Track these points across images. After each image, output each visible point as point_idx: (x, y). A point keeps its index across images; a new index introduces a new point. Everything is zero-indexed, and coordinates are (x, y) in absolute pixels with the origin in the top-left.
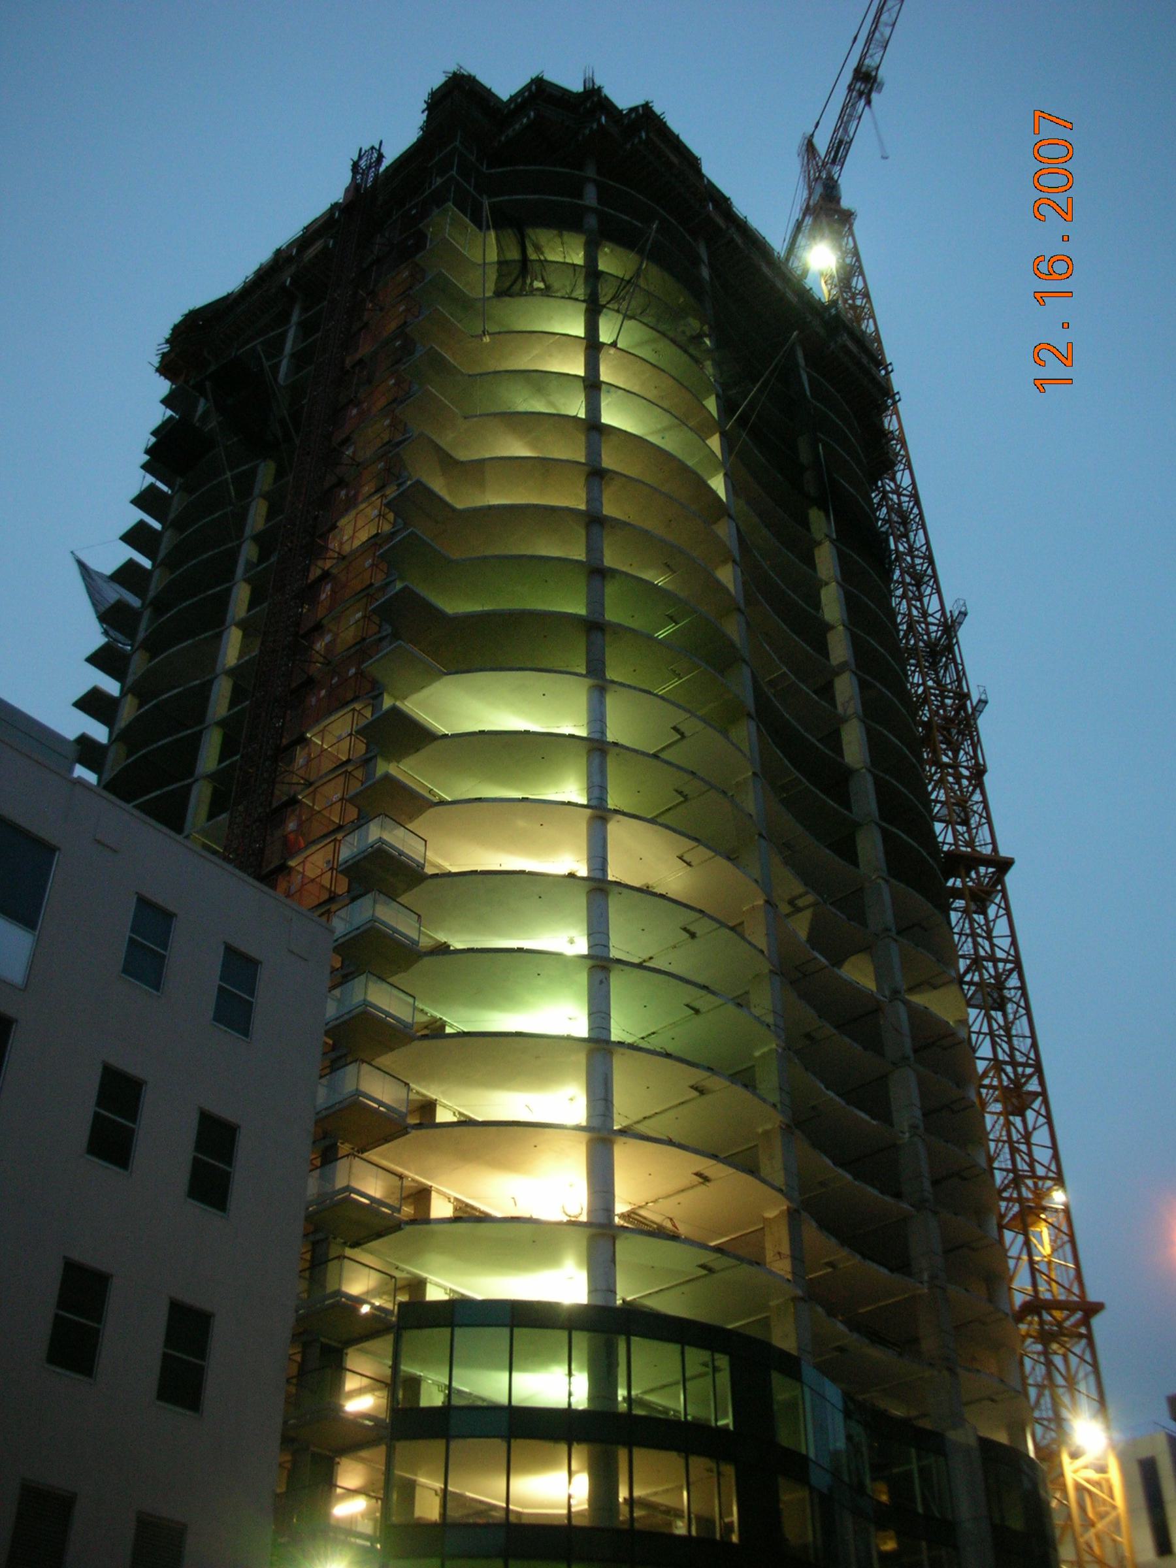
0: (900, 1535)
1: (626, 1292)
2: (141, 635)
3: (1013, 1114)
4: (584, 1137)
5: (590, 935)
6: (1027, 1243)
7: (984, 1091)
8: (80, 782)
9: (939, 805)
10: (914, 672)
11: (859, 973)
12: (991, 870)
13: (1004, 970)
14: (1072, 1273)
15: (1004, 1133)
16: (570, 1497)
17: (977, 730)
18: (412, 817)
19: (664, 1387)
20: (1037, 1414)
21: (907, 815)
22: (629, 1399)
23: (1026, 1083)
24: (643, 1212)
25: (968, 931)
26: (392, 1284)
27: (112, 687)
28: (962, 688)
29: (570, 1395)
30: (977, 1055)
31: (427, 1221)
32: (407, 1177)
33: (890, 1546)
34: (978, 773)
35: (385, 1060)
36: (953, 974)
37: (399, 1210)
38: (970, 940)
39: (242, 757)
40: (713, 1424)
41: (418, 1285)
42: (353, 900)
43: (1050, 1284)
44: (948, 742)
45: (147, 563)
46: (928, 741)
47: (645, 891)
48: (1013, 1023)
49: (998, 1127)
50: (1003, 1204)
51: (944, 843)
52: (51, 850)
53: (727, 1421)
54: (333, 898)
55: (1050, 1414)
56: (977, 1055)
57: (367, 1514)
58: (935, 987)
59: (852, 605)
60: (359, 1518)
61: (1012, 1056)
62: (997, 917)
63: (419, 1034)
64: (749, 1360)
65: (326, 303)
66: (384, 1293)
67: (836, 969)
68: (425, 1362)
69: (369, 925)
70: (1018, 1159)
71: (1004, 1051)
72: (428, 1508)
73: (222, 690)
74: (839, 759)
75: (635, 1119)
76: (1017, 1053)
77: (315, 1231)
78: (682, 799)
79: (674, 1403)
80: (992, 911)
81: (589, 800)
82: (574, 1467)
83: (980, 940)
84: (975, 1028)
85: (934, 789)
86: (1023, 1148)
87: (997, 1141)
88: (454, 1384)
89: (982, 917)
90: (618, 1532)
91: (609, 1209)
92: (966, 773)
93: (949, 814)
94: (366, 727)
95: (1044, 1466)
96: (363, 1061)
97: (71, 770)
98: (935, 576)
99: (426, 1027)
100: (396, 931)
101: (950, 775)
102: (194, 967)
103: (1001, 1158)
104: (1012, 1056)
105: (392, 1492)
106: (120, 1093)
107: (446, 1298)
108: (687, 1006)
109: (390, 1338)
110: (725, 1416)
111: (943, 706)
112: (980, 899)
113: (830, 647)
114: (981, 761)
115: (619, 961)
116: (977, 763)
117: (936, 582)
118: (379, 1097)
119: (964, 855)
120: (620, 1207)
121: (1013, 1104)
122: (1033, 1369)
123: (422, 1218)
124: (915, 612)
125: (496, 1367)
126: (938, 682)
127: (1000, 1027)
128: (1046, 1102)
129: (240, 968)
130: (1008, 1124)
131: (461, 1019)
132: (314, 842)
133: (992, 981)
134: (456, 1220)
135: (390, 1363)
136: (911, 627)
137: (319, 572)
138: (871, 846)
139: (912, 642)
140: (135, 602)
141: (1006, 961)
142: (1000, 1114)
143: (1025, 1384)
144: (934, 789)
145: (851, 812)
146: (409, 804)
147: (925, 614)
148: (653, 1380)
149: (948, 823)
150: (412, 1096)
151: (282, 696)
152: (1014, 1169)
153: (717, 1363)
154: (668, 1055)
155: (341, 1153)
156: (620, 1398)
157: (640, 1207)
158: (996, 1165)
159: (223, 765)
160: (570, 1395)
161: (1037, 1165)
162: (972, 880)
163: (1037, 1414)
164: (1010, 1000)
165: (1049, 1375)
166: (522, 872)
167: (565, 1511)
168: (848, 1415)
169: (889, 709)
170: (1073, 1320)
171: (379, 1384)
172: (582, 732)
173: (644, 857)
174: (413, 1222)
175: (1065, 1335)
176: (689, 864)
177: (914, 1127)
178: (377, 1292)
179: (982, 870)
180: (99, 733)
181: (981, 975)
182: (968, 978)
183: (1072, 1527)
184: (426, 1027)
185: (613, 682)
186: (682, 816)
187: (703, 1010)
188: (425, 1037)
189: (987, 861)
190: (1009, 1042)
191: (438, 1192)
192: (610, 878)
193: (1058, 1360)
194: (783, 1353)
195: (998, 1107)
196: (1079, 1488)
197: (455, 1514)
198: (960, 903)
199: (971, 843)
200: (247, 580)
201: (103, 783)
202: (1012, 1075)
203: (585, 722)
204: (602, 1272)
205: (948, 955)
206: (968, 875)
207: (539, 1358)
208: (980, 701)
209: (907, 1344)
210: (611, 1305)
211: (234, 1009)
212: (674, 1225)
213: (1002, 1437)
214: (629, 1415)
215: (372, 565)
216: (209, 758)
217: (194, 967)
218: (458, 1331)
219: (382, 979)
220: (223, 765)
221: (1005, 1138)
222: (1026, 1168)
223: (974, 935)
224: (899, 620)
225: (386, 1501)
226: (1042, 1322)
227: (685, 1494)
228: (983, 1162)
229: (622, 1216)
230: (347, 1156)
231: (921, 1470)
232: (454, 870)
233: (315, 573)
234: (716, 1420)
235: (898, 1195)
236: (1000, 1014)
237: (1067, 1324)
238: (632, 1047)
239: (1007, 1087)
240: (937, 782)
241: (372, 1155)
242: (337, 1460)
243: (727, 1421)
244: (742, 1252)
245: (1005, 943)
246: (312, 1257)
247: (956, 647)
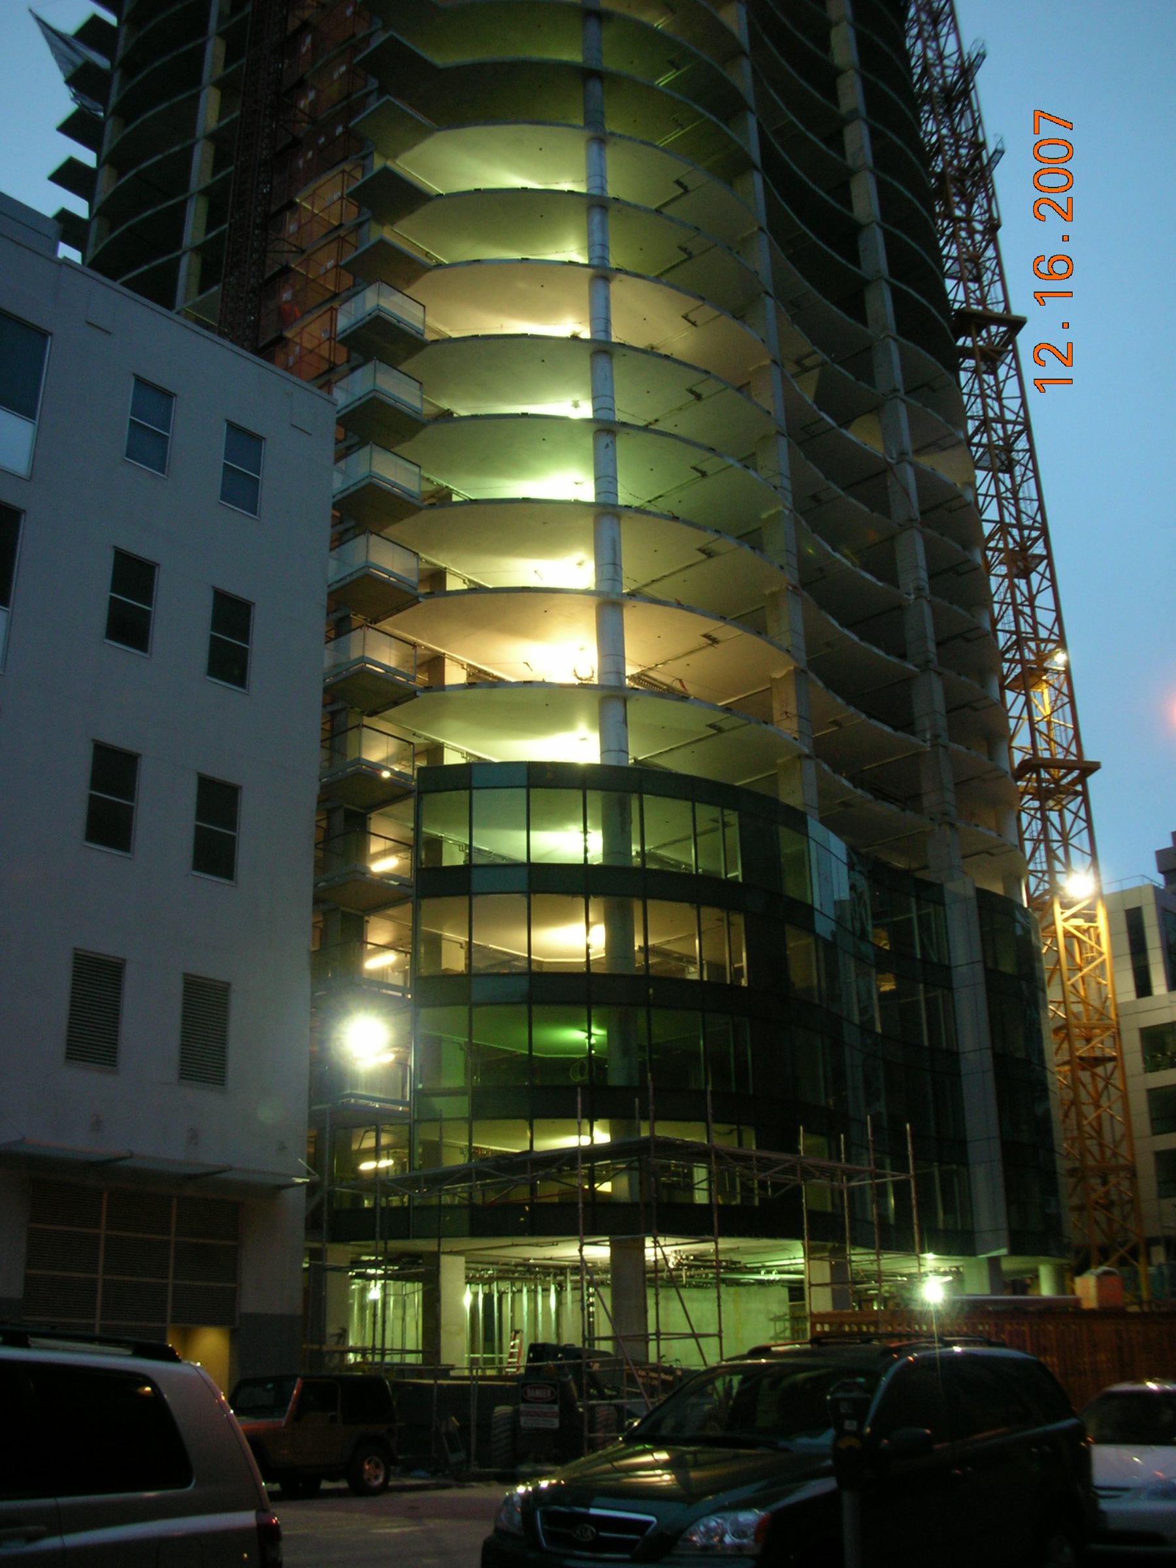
0: (898, 978)
1: (638, 751)
2: (113, 100)
3: (1019, 577)
4: (593, 601)
5: (594, 399)
6: (1028, 703)
7: (989, 554)
8: (67, 262)
9: (950, 262)
10: (928, 119)
11: (864, 436)
12: (1002, 329)
13: (1013, 432)
14: (1071, 733)
15: (1008, 595)
16: (588, 947)
17: (991, 181)
18: (409, 282)
19: (675, 842)
20: (1031, 867)
21: (918, 271)
22: (642, 854)
23: (1031, 546)
24: (652, 674)
25: (977, 392)
26: (408, 749)
27: (88, 158)
28: (977, 138)
29: (586, 851)
30: (984, 517)
31: (442, 687)
32: (420, 645)
33: (888, 987)
34: (993, 226)
35: (393, 531)
36: (962, 436)
37: (414, 679)
38: (979, 400)
39: (230, 225)
40: (723, 877)
41: (436, 750)
42: (353, 370)
43: (1049, 744)
44: (962, 194)
45: (112, 19)
46: (941, 193)
47: (650, 352)
48: (1020, 485)
49: (1002, 589)
50: (1006, 665)
51: (955, 301)
52: (44, 334)
53: (737, 873)
54: (332, 368)
55: (1045, 867)
56: (984, 517)
57: (396, 967)
58: (943, 449)
59: (865, 48)
60: (390, 971)
61: (1018, 519)
62: (1007, 378)
63: (426, 503)
64: (759, 816)
65: (226, 226)
66: (403, 759)
67: (844, 431)
68: (446, 824)
69: (371, 395)
70: (1022, 620)
71: (1010, 514)
72: (454, 960)
73: (202, 157)
74: (849, 214)
75: (643, 583)
76: (1024, 516)
77: (327, 800)
78: (686, 256)
79: (686, 857)
80: (1002, 371)
81: (590, 259)
82: (591, 920)
83: (989, 401)
84: (982, 490)
85: (945, 245)
86: (1027, 610)
87: (1002, 603)
88: (475, 844)
89: (992, 377)
90: (632, 978)
91: (620, 673)
92: (979, 227)
93: (961, 271)
94: (358, 189)
95: (1037, 915)
96: (372, 533)
97: (55, 250)
98: (952, 12)
99: (432, 496)
100: (394, 485)
101: (963, 229)
102: (198, 444)
103: (1005, 620)
104: (1018, 519)
105: (420, 946)
106: (133, 576)
107: (463, 761)
108: (694, 468)
109: (411, 803)
110: (736, 869)
111: (957, 155)
112: (990, 359)
113: (839, 93)
114: (995, 215)
115: (624, 424)
116: (991, 216)
117: (954, 20)
118: (389, 567)
119: (975, 314)
120: (630, 670)
121: (1018, 567)
122: (1030, 824)
123: (437, 684)
124: (930, 54)
125: (517, 827)
126: (953, 131)
127: (1007, 490)
128: (1050, 565)
129: (244, 443)
130: (1012, 587)
131: (467, 488)
132: (309, 312)
133: (1001, 443)
134: (470, 685)
135: (412, 825)
136: (926, 70)
137: (297, 23)
138: (881, 304)
139: (926, 87)
140: (103, 63)
141: (1015, 423)
142: (1004, 577)
143: (1022, 840)
144: (945, 245)
145: (859, 268)
146: (402, 269)
147: (941, 56)
148: (666, 836)
149: (959, 279)
150: (423, 566)
151: (271, 153)
152: (1017, 631)
153: (726, 819)
154: (675, 518)
155: (355, 624)
156: (634, 853)
157: (650, 669)
158: (999, 627)
159: (218, 177)
160: (586, 851)
161: (1040, 628)
162: (982, 339)
163: (1031, 867)
164: (1018, 462)
165: (1044, 830)
166: (525, 336)
167: (584, 960)
168: (851, 867)
169: (902, 157)
170: (1070, 778)
171: (403, 846)
172: (580, 188)
173: (649, 318)
174: (428, 689)
175: (1061, 793)
176: (694, 324)
177: (919, 589)
178: (398, 759)
179: (993, 329)
180: (80, 207)
181: (989, 437)
182: (976, 440)
183: (1060, 970)
184: (432, 496)
185: (612, 134)
186: (688, 270)
187: (709, 473)
188: (432, 505)
189: (998, 320)
190: (1016, 505)
191: (452, 659)
192: (614, 340)
193: (1054, 816)
194: (791, 810)
195: (1003, 570)
196: (1068, 935)
197: (480, 965)
198: (970, 363)
199: (982, 301)
200: (221, 35)
201: (88, 261)
202: (1018, 538)
203: (584, 177)
204: (613, 739)
205: (959, 415)
206: (979, 334)
207: (555, 818)
208: (996, 151)
209: (911, 799)
210: (623, 764)
211: (241, 488)
212: (683, 686)
213: (998, 889)
214: (642, 871)
215: (354, 13)
216: (194, 230)
217: (198, 444)
218: (475, 792)
219: (387, 449)
220: (218, 177)
221: (1009, 601)
222: (1029, 630)
223: (983, 396)
224: (913, 63)
225: (414, 955)
226: (1039, 780)
227: (697, 942)
228: (987, 625)
229: (632, 678)
230: (361, 627)
231: (920, 918)
232: (455, 335)
233: (293, 24)
234: (726, 874)
235: (903, 656)
236: (1007, 476)
237: (1064, 782)
238: (639, 510)
239: (1012, 550)
240: (949, 237)
241: (385, 625)
242: (366, 918)
243: (737, 873)
244: (753, 708)
245: (1015, 405)
246: (332, 726)
247: (973, 93)
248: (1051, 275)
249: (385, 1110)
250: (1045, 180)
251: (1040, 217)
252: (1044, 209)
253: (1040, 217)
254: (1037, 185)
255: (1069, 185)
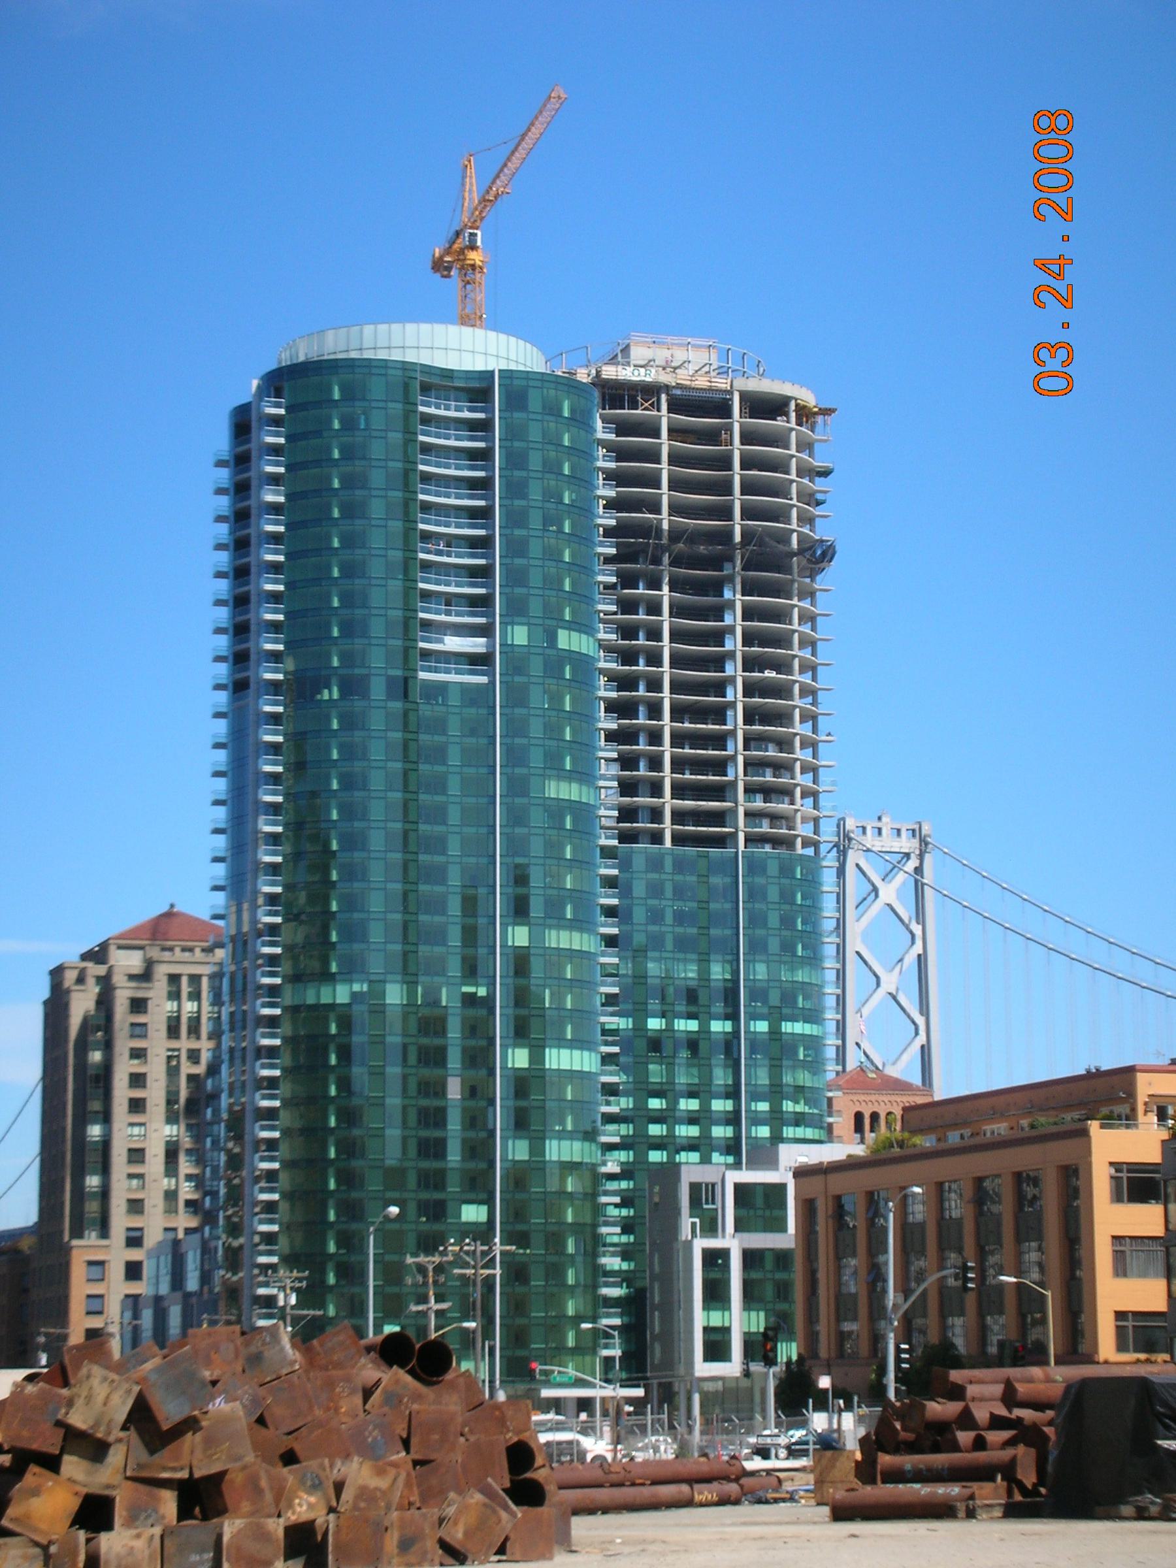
250: (1046, 180)
251: (1040, 304)
252: (1044, 209)
253: (1040, 304)
254: (1037, 185)
255: (1069, 186)
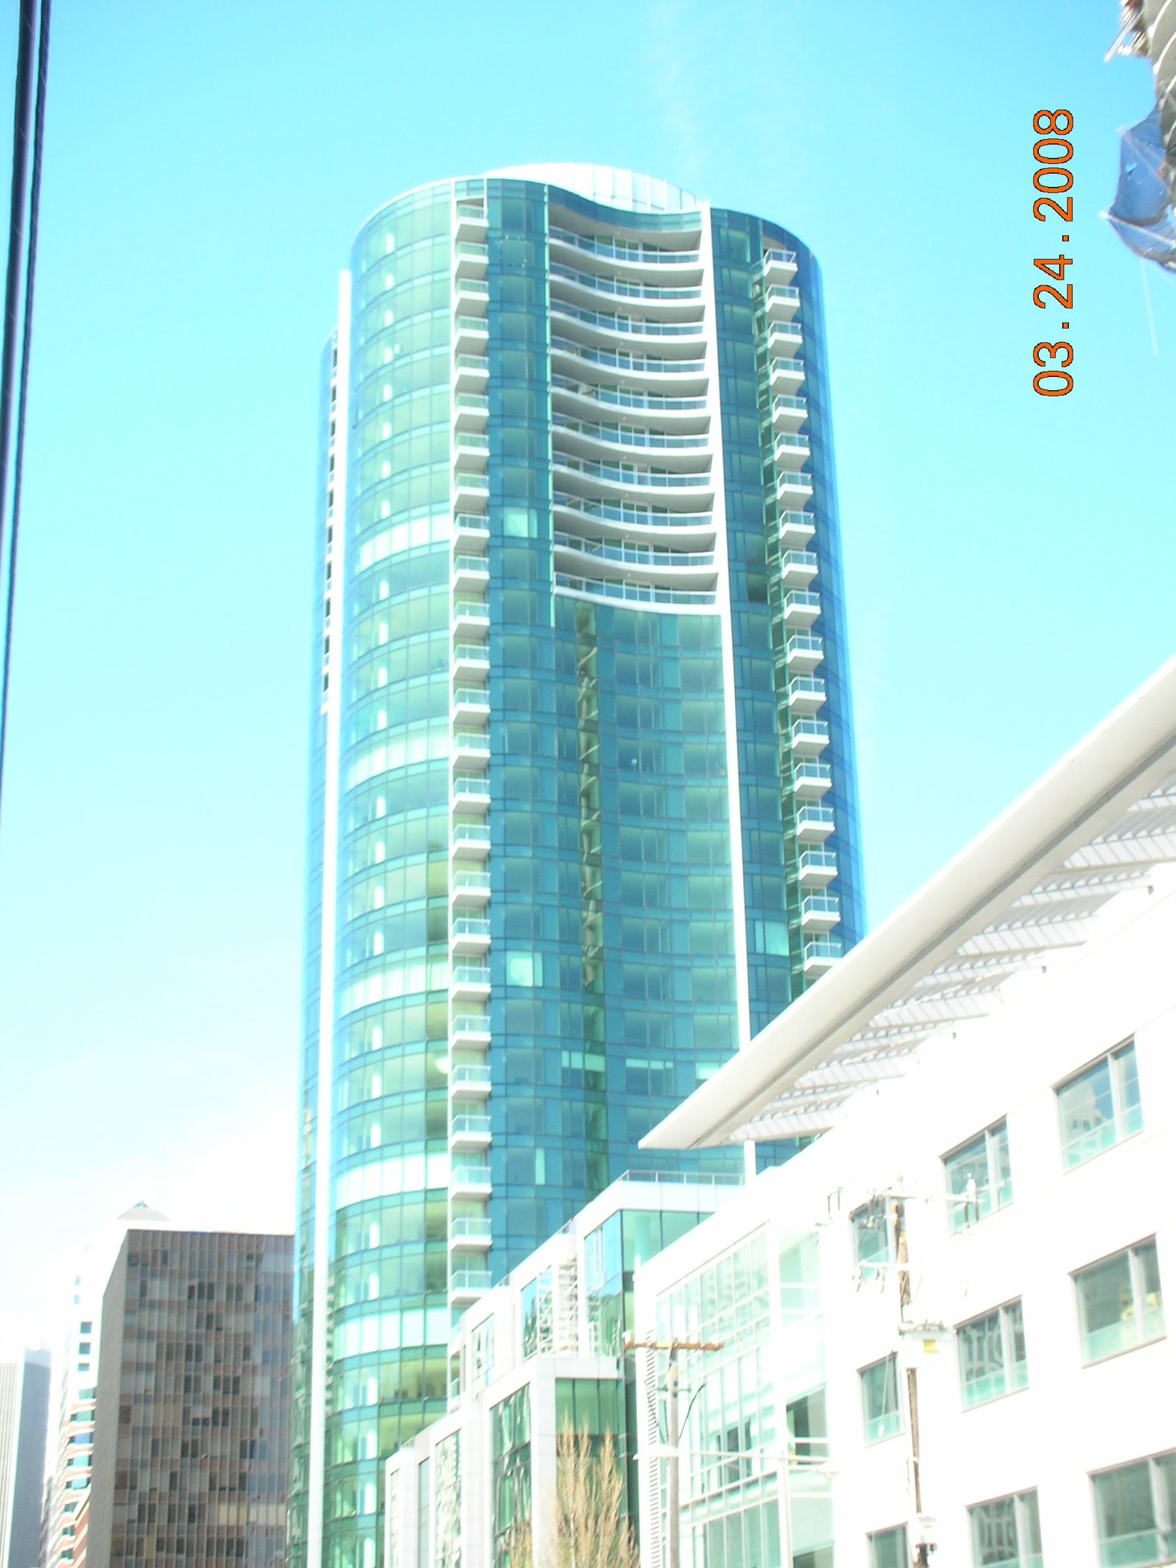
248: (1053, 128)
249: (42, 1487)
250: (1045, 180)
251: (1041, 217)
253: (1041, 217)
255: (1069, 185)
